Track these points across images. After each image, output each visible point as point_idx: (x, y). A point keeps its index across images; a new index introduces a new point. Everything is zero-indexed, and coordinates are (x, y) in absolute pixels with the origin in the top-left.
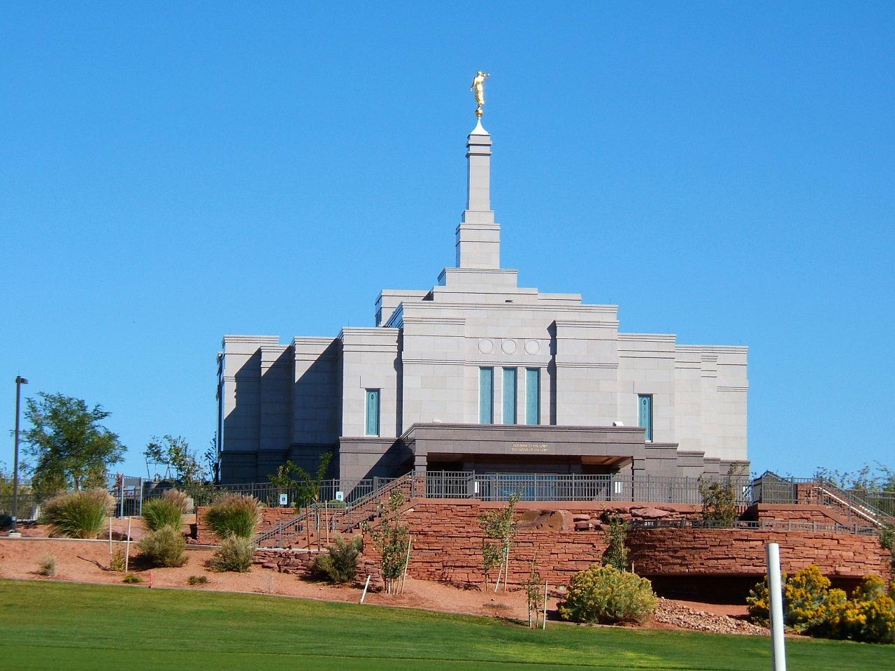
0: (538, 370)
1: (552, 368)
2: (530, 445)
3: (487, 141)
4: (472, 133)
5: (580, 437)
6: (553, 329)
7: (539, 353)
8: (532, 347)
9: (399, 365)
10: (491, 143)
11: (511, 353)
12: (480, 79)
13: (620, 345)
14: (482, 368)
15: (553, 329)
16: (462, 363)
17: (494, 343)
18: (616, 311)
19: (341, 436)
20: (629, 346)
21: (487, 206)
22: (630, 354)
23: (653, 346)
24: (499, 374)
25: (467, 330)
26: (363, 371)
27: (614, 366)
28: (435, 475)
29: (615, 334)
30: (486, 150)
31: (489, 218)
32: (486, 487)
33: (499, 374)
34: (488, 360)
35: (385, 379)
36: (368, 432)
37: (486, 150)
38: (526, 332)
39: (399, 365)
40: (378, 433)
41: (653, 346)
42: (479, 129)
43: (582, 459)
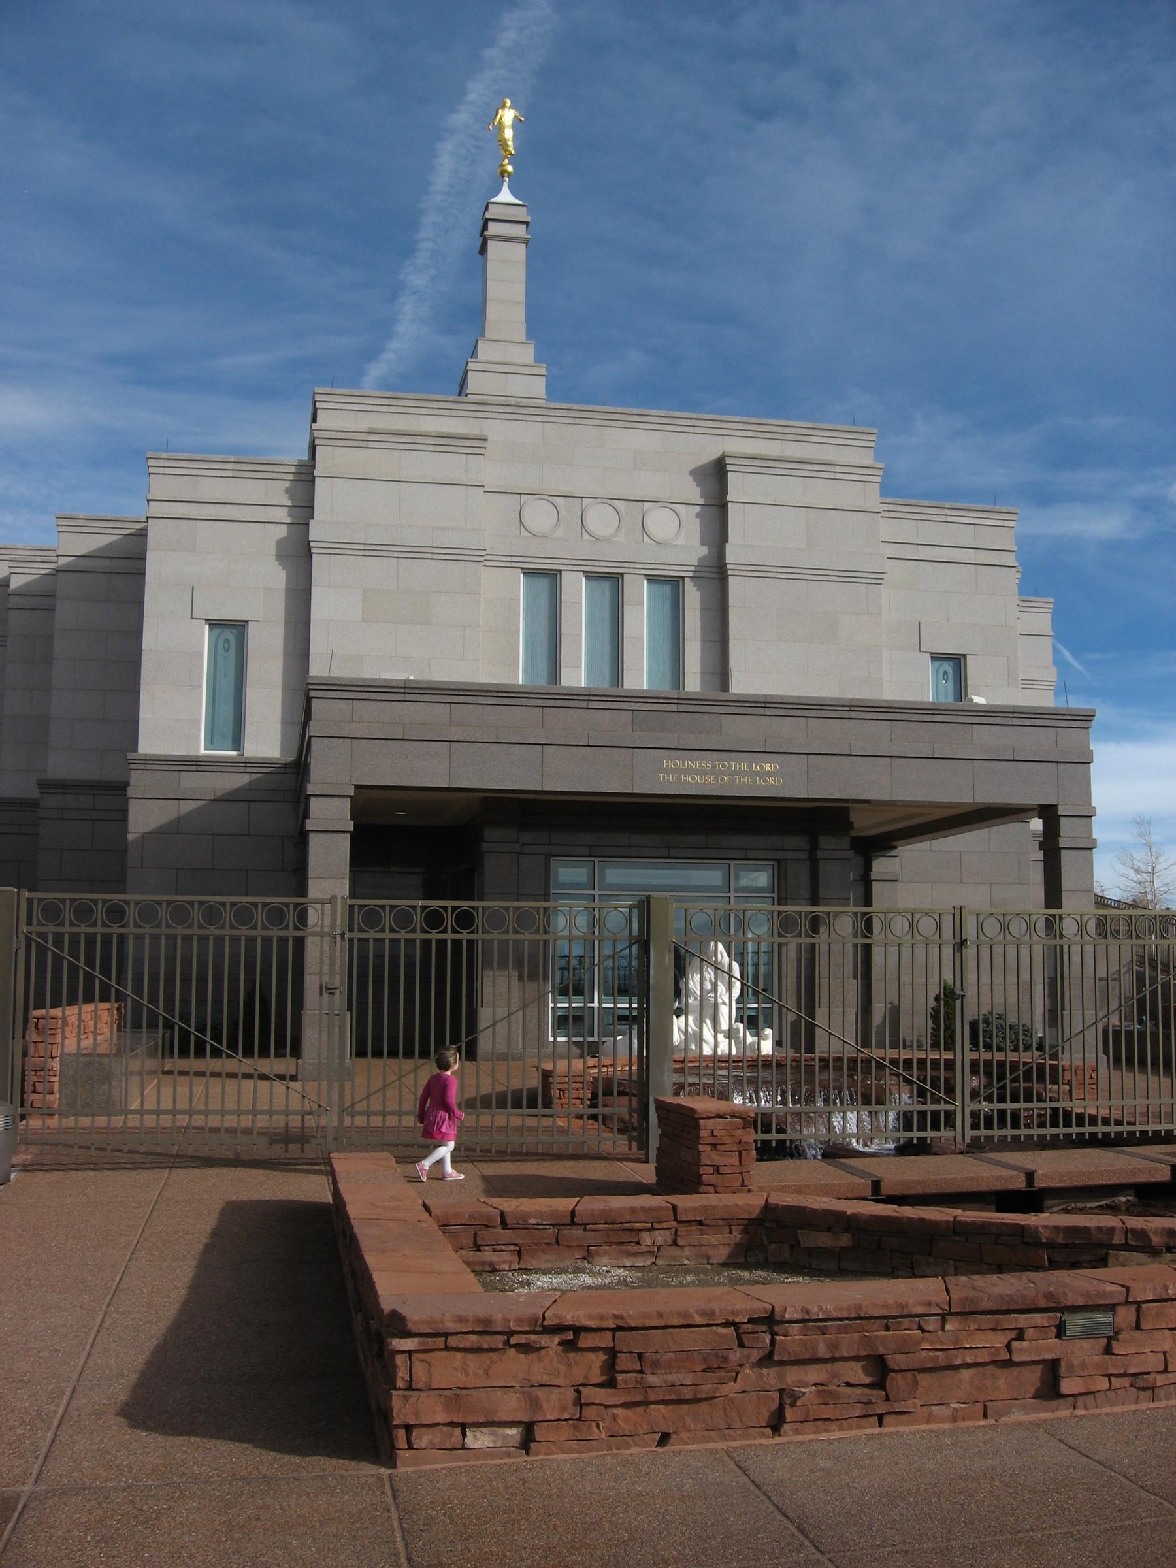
0: (676, 583)
1: (716, 574)
2: (721, 763)
3: (522, 214)
4: (493, 200)
5: (877, 736)
6: (716, 475)
7: (677, 539)
8: (662, 523)
9: (299, 555)
10: (528, 219)
11: (606, 534)
12: (508, 116)
13: (887, 529)
14: (528, 573)
15: (716, 475)
16: (470, 556)
17: (562, 512)
18: (872, 444)
19: (136, 751)
20: (906, 530)
21: (520, 333)
22: (908, 552)
23: (964, 535)
24: (577, 592)
25: (489, 471)
26: (207, 574)
27: (874, 579)
28: (1067, 1114)
29: (872, 497)
30: (520, 231)
31: (525, 354)
32: (1154, 1035)
33: (577, 592)
34: (547, 553)
35: (259, 595)
36: (211, 743)
37: (520, 231)
38: (648, 484)
39: (299, 555)
40: (237, 744)
41: (964, 535)
42: (506, 196)
43: (853, 817)
